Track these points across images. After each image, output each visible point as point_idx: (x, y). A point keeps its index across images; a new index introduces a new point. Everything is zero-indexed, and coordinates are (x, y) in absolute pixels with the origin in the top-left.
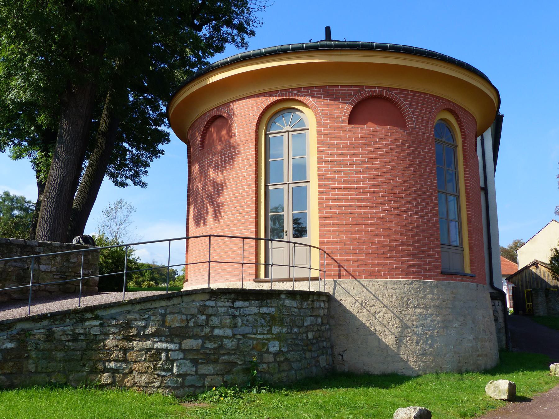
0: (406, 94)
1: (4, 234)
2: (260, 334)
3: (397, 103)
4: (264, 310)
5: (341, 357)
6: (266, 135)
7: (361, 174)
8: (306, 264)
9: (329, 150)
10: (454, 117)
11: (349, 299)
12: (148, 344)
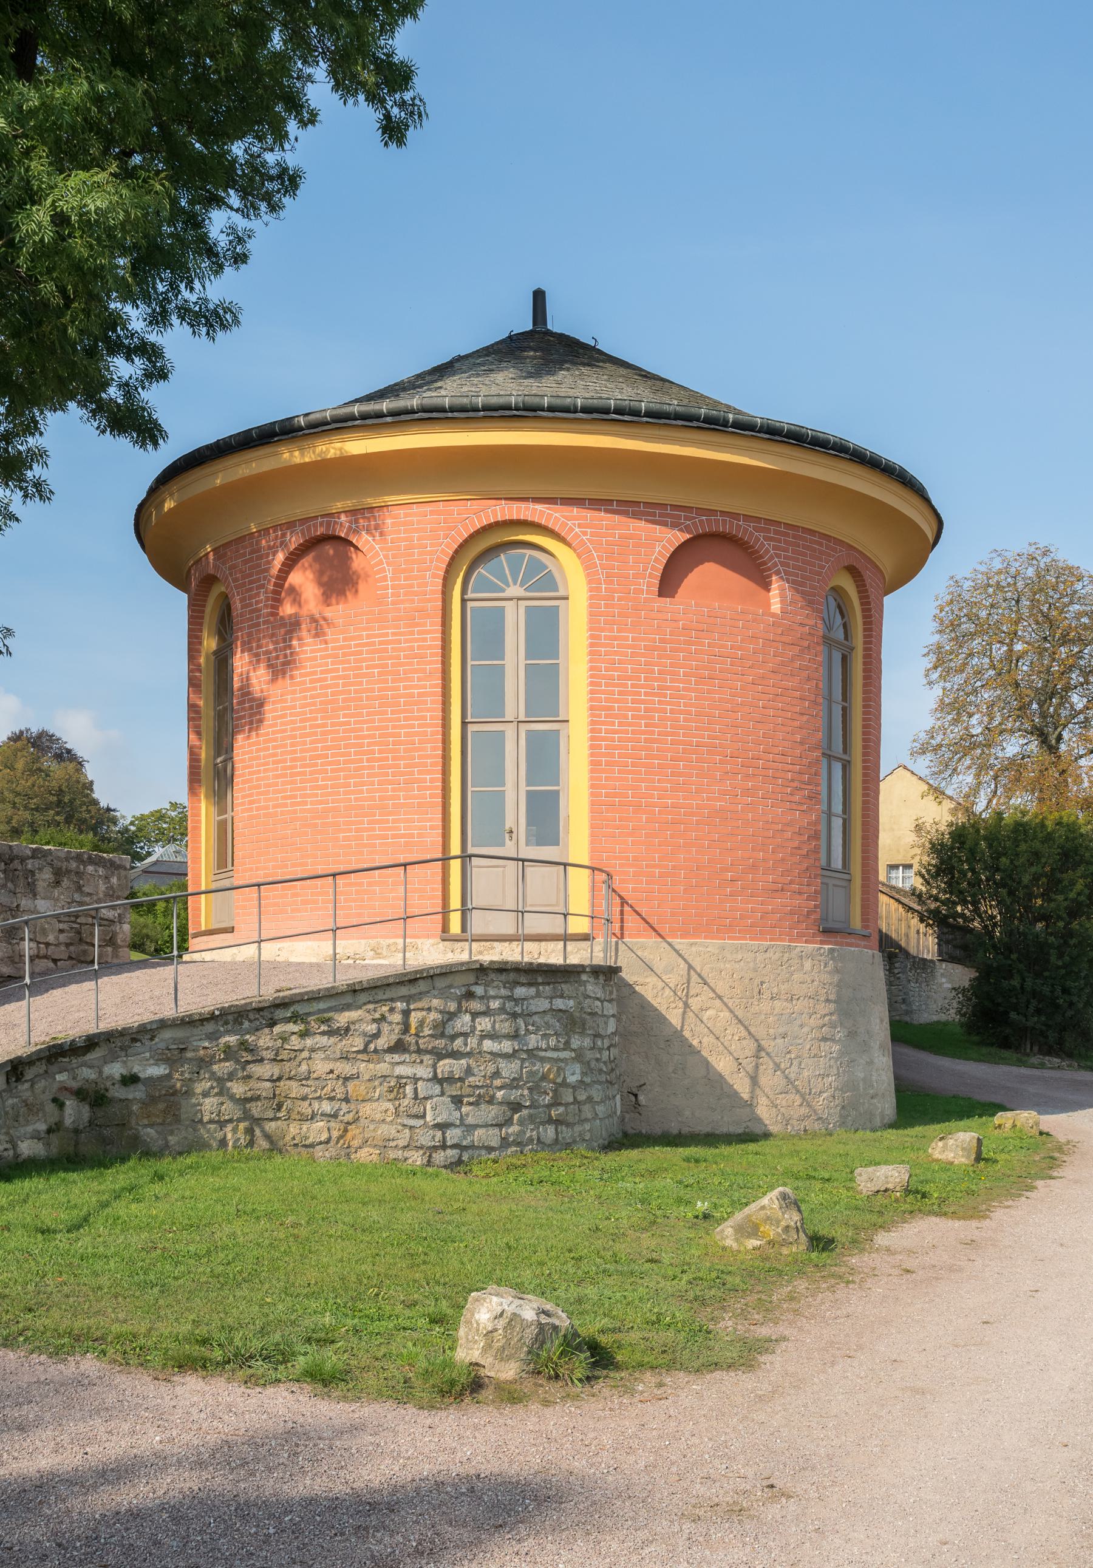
0: (776, 532)
1: (16, 832)
2: (553, 1050)
3: (757, 552)
4: (559, 1004)
5: (633, 1099)
6: (464, 601)
7: (681, 712)
8: (557, 905)
9: (616, 653)
10: (855, 581)
11: (652, 980)
12: (383, 1068)
